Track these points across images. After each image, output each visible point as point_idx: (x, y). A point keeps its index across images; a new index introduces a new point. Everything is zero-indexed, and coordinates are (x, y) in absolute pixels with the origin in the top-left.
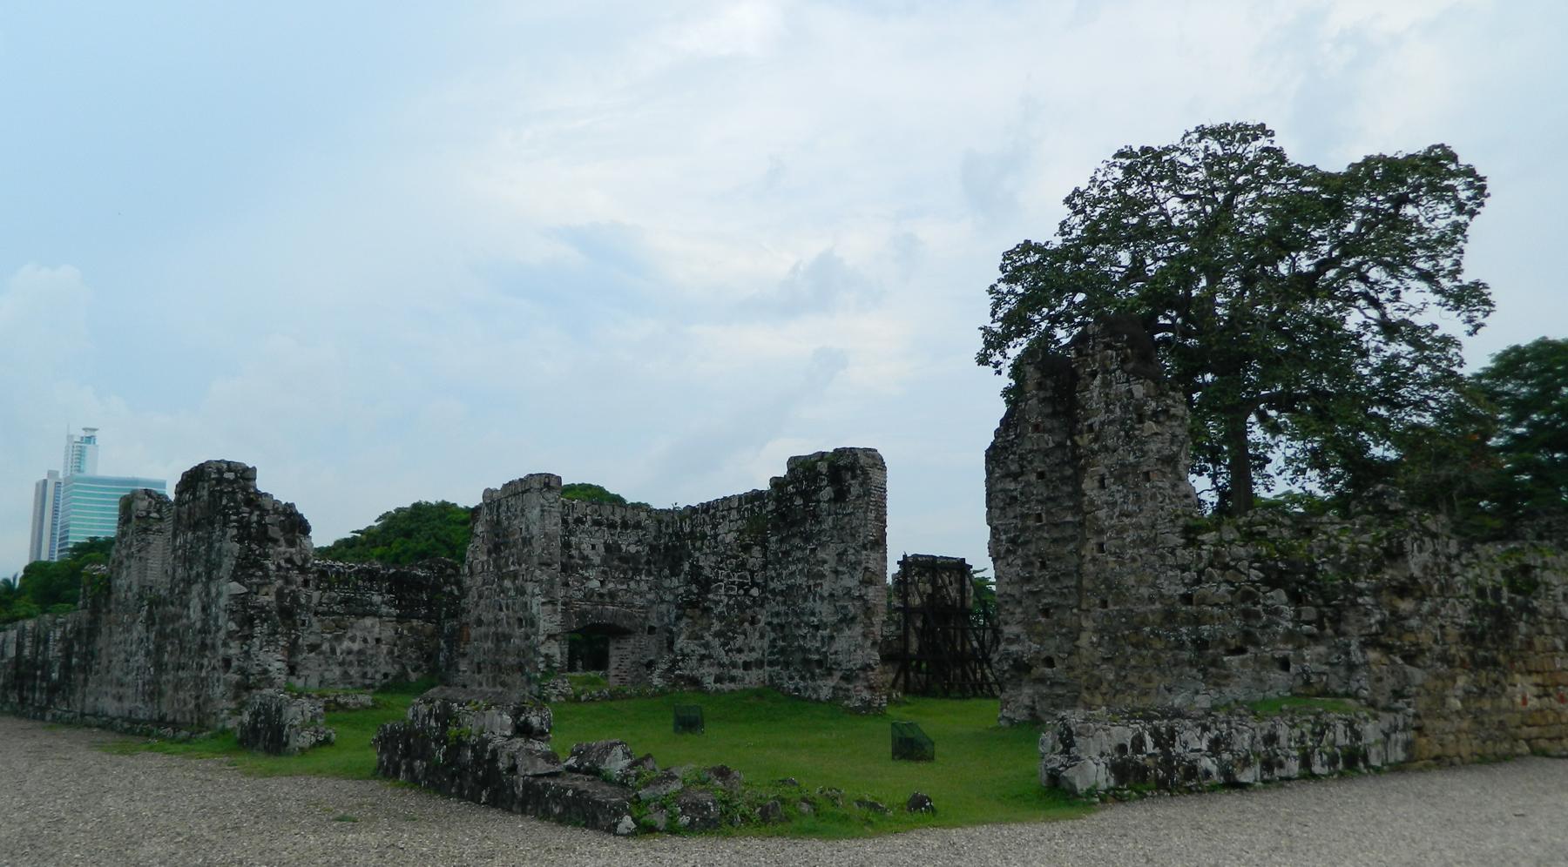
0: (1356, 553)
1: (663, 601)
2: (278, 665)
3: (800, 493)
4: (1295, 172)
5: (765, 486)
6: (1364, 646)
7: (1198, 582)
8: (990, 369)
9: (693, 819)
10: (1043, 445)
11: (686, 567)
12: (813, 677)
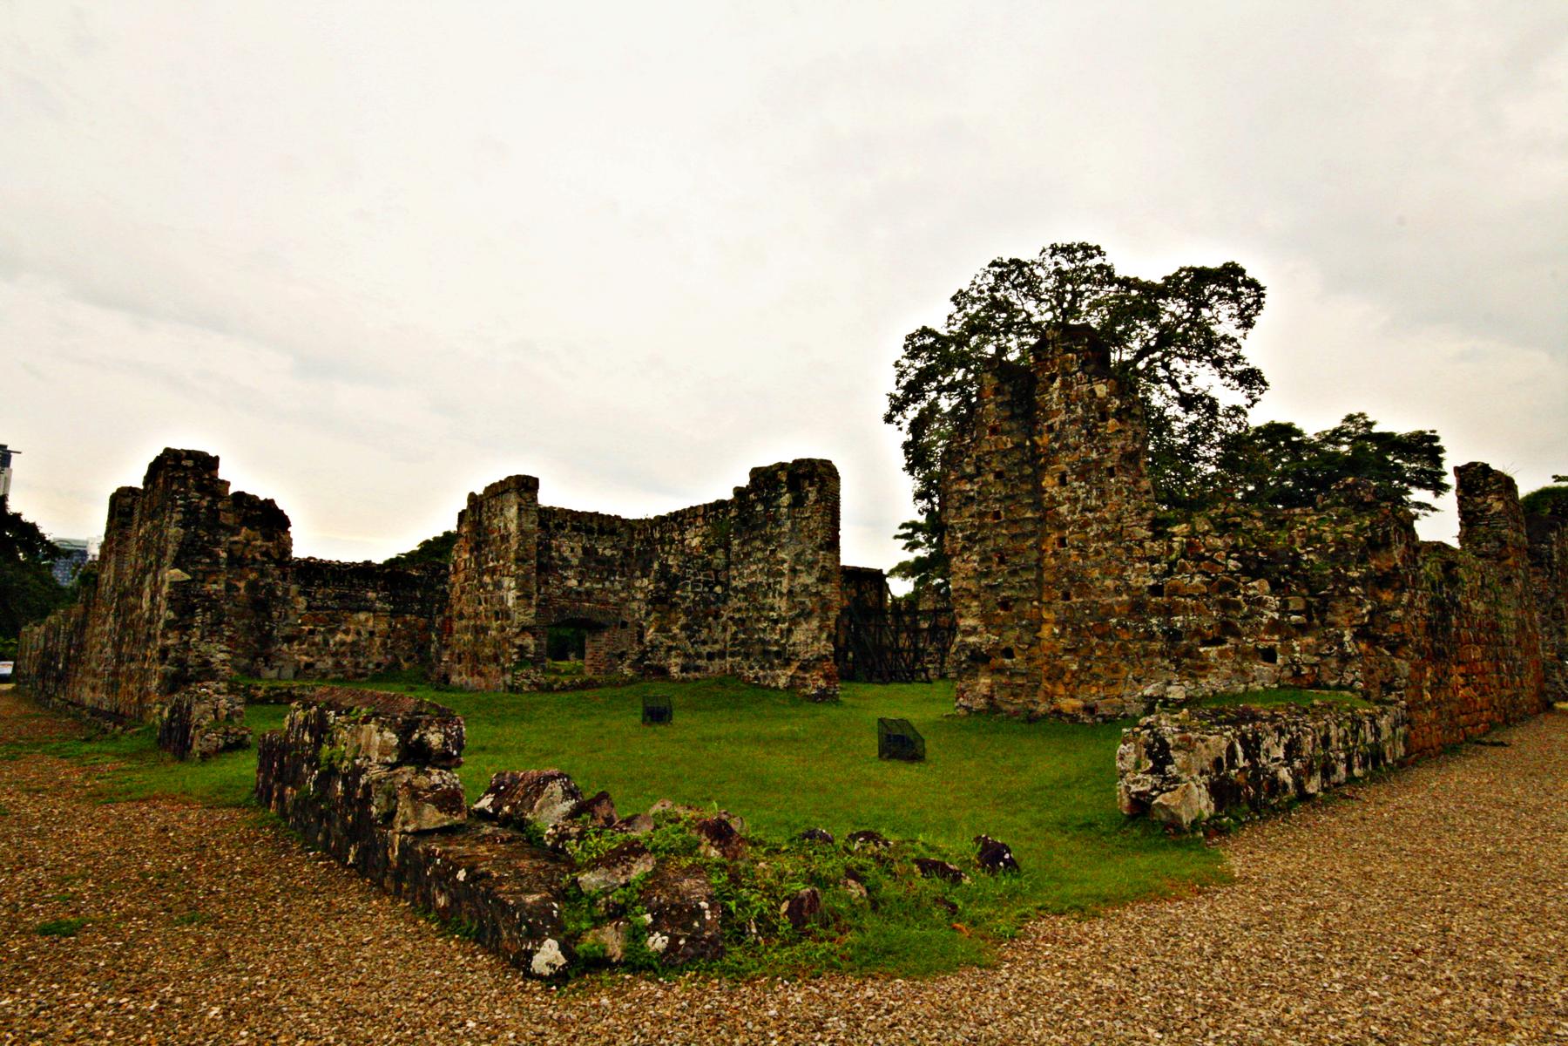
0: (1342, 544)
1: (634, 599)
2: (222, 656)
3: (760, 500)
4: (1127, 283)
5: (728, 495)
6: (1356, 637)
7: (1169, 573)
8: (893, 426)
9: (674, 939)
10: (1001, 446)
11: (656, 566)
12: (772, 667)
